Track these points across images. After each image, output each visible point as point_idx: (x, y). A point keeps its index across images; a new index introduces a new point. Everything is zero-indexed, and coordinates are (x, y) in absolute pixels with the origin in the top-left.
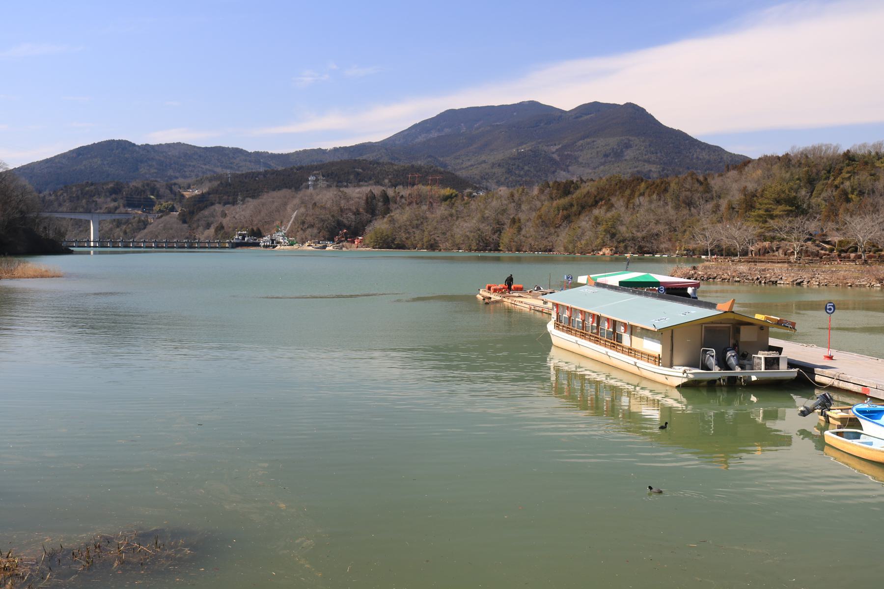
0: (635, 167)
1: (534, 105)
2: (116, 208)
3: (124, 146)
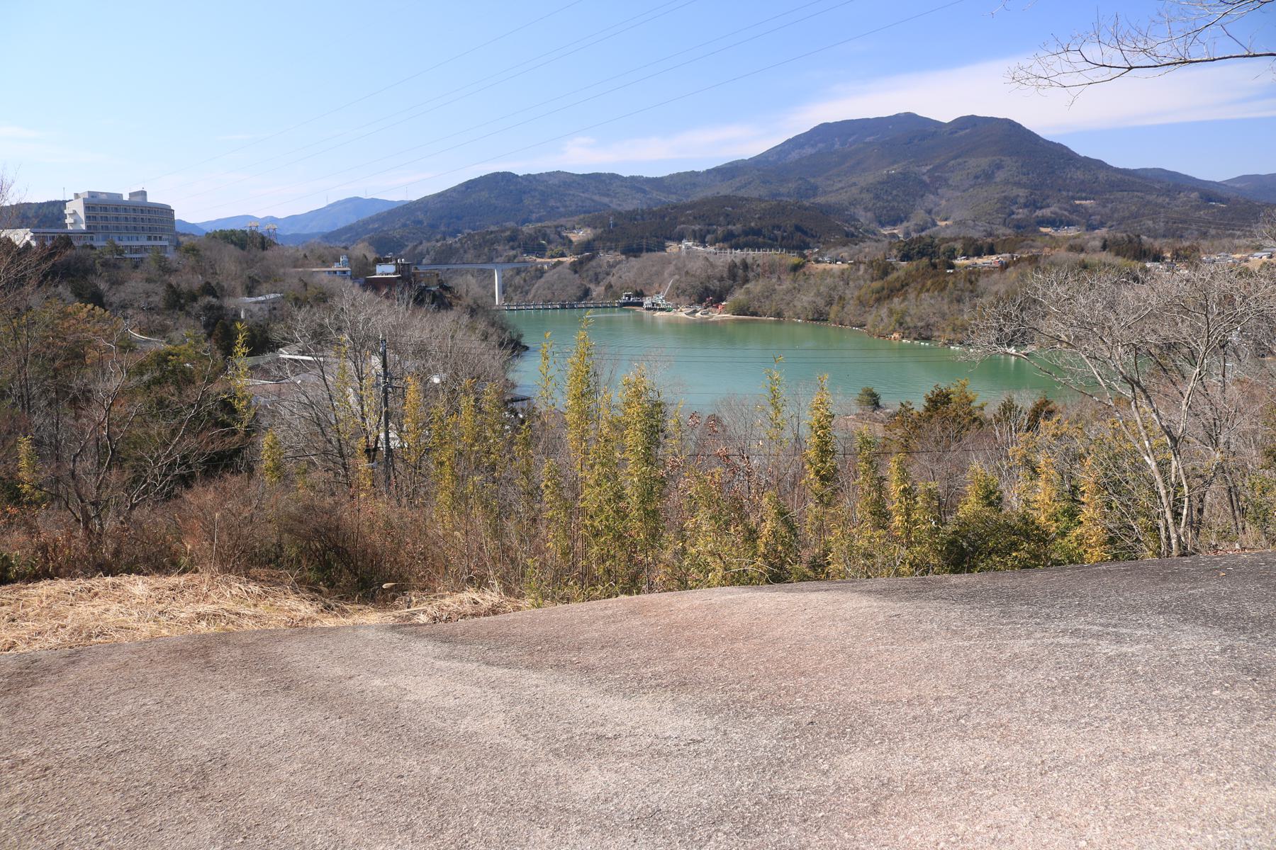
0: (1003, 192)
1: (910, 117)
2: (515, 257)
3: (507, 177)
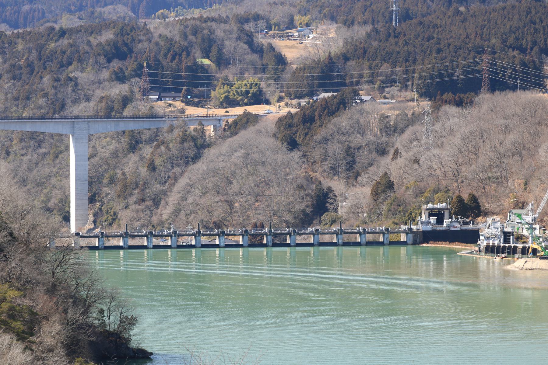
2: (126, 101)
